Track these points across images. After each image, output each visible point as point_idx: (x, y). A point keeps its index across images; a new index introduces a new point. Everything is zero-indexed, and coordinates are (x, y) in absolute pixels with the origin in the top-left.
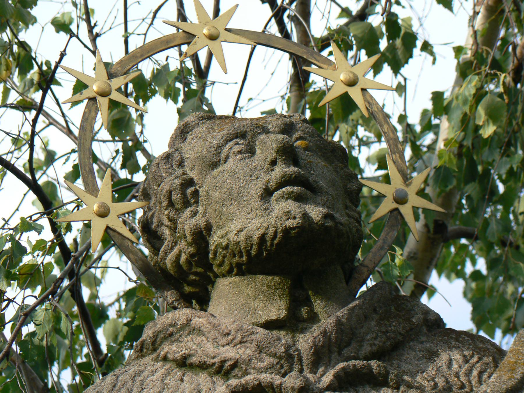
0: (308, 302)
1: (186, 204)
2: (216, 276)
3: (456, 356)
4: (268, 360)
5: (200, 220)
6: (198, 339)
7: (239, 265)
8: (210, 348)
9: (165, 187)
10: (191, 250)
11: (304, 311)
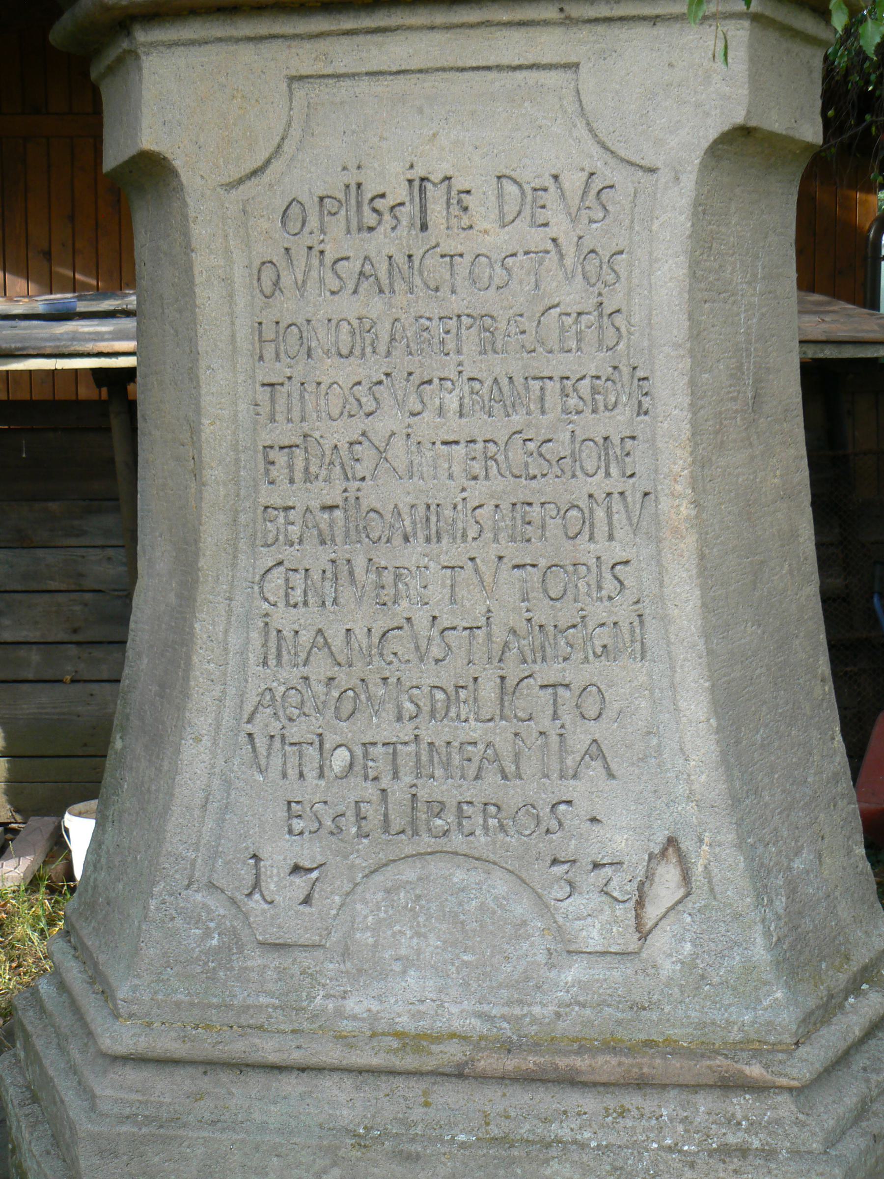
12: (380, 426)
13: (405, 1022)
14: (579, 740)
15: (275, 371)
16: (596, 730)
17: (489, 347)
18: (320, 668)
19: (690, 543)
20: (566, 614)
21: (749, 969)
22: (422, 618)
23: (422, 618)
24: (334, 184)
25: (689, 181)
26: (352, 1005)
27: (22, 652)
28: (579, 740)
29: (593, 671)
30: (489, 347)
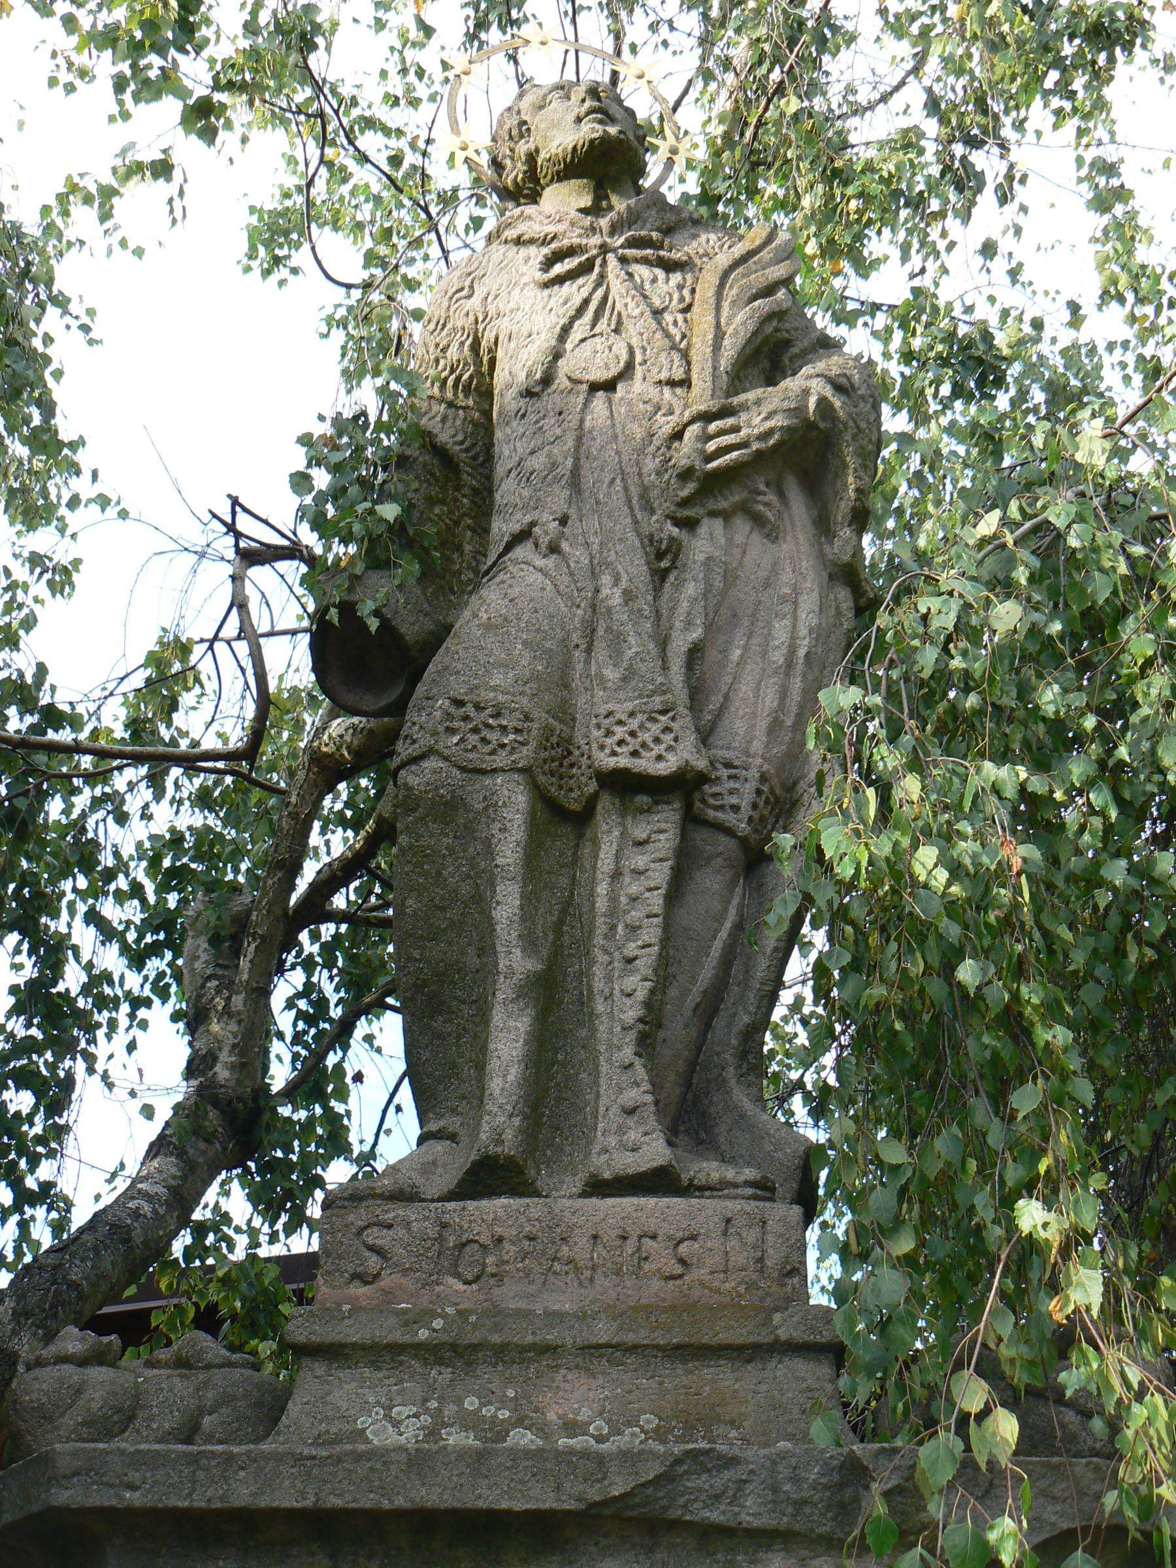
0: (607, 198)
1: (522, 136)
2: (543, 188)
3: (713, 237)
4: (578, 231)
5: (532, 146)
6: (528, 224)
7: (558, 172)
8: (537, 227)
9: (507, 127)
10: (525, 168)
11: (604, 204)
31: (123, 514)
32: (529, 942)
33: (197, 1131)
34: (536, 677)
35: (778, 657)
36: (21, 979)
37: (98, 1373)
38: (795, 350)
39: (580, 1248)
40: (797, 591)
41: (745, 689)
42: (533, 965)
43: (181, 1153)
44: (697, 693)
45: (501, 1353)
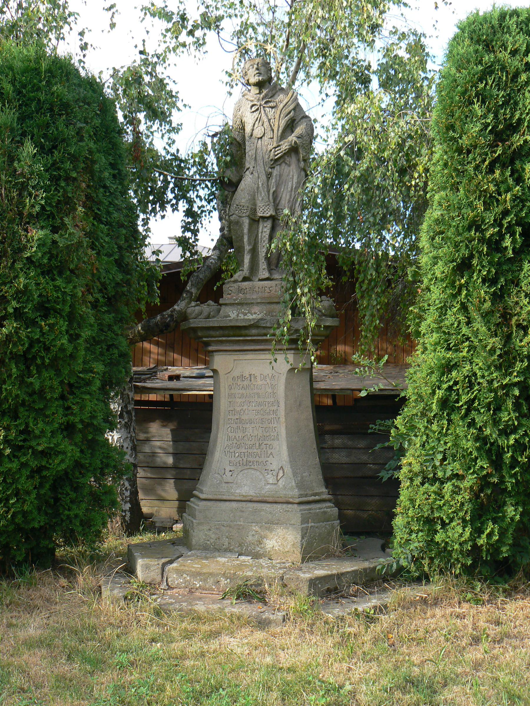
12: (244, 408)
13: (244, 494)
14: (269, 452)
15: (230, 400)
16: (272, 451)
17: (259, 397)
18: (235, 441)
19: (284, 424)
20: (268, 434)
21: (292, 486)
22: (249, 434)
23: (249, 434)
24: (239, 375)
25: (285, 375)
26: (237, 491)
27: (185, 471)
28: (269, 452)
29: (271, 442)
30: (259, 397)
31: (190, 107)
32: (249, 244)
33: (222, 244)
34: (249, 199)
35: (289, 189)
36: (185, 209)
37: (197, 308)
38: (297, 121)
39: (257, 289)
40: (293, 176)
41: (284, 195)
42: (251, 247)
43: (219, 250)
44: (275, 200)
45: (246, 304)
